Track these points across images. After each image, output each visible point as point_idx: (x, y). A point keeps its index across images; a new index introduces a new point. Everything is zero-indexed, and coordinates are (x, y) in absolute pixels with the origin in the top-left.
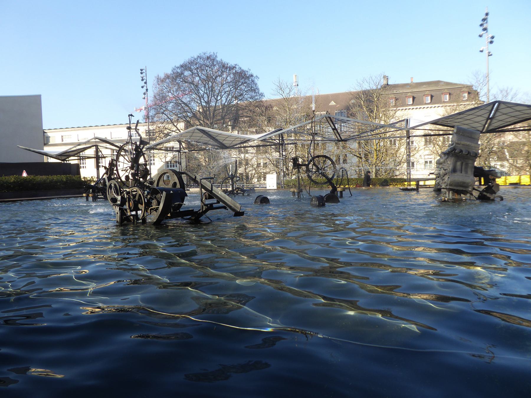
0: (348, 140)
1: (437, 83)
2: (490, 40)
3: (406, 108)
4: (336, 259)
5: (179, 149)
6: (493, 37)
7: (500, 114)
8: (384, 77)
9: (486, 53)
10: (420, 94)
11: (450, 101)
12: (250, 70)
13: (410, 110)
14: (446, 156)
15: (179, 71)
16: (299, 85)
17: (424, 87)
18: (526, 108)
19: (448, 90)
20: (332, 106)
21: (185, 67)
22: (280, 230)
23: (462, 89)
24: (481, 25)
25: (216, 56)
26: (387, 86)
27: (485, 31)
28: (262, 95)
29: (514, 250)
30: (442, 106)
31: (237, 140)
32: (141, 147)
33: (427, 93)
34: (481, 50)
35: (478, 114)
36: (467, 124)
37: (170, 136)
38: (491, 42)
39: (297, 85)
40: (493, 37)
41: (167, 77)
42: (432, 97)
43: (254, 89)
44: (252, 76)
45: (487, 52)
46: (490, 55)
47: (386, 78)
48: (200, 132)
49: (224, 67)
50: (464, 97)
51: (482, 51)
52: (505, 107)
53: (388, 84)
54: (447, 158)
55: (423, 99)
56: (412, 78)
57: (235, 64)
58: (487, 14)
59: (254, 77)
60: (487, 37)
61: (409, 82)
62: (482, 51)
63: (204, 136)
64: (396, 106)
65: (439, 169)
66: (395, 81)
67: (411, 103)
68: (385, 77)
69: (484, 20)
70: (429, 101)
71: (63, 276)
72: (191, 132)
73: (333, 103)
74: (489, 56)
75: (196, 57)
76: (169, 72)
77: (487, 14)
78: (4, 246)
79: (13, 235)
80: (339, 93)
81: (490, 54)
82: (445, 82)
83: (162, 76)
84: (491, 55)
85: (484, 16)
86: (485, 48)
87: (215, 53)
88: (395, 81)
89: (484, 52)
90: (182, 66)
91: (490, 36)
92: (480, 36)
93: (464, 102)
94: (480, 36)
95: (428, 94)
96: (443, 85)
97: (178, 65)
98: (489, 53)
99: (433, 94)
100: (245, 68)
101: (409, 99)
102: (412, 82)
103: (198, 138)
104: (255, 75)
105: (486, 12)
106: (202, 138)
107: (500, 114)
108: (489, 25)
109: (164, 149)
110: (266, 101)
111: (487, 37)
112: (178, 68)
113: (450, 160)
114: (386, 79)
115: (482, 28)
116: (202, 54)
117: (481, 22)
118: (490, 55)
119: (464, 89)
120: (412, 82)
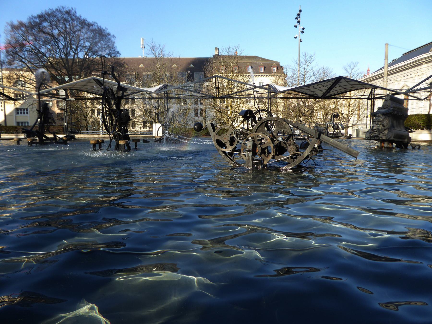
1: (255, 57)
2: (301, 30)
3: (270, 75)
5: (65, 97)
6: (303, 29)
8: (216, 48)
9: (298, 39)
10: (243, 65)
12: (107, 29)
13: (262, 77)
14: (384, 117)
15: (38, 20)
17: (246, 60)
18: (357, 83)
20: (141, 68)
21: (42, 17)
23: (273, 64)
24: (296, 18)
25: (75, 12)
26: (217, 57)
27: (299, 24)
34: (296, 37)
38: (303, 32)
39: (144, 48)
40: (303, 29)
41: (21, 24)
42: (265, 68)
43: (111, 47)
44: (109, 34)
48: (95, 82)
49: (84, 24)
51: (296, 38)
52: (344, 81)
53: (218, 55)
54: (385, 118)
55: (258, 69)
57: (94, 21)
58: (300, 11)
59: (111, 36)
60: (300, 27)
62: (296, 38)
64: (238, 72)
65: (378, 125)
66: (248, 53)
68: (216, 49)
69: (298, 15)
70: (263, 71)
71: (370, 246)
72: (87, 81)
74: (300, 42)
76: (25, 20)
77: (300, 11)
80: (131, 59)
81: (301, 41)
82: (260, 58)
83: (16, 23)
84: (302, 41)
85: (298, 12)
86: (297, 36)
87: (74, 8)
88: (248, 53)
91: (302, 27)
92: (295, 26)
94: (295, 26)
95: (262, 66)
97: (35, 15)
98: (300, 40)
99: (265, 65)
100: (103, 27)
104: (112, 34)
105: (300, 9)
106: (85, 87)
108: (301, 19)
110: (124, 59)
111: (300, 27)
112: (35, 17)
113: (387, 119)
114: (217, 50)
115: (296, 21)
116: (61, 8)
117: (296, 16)
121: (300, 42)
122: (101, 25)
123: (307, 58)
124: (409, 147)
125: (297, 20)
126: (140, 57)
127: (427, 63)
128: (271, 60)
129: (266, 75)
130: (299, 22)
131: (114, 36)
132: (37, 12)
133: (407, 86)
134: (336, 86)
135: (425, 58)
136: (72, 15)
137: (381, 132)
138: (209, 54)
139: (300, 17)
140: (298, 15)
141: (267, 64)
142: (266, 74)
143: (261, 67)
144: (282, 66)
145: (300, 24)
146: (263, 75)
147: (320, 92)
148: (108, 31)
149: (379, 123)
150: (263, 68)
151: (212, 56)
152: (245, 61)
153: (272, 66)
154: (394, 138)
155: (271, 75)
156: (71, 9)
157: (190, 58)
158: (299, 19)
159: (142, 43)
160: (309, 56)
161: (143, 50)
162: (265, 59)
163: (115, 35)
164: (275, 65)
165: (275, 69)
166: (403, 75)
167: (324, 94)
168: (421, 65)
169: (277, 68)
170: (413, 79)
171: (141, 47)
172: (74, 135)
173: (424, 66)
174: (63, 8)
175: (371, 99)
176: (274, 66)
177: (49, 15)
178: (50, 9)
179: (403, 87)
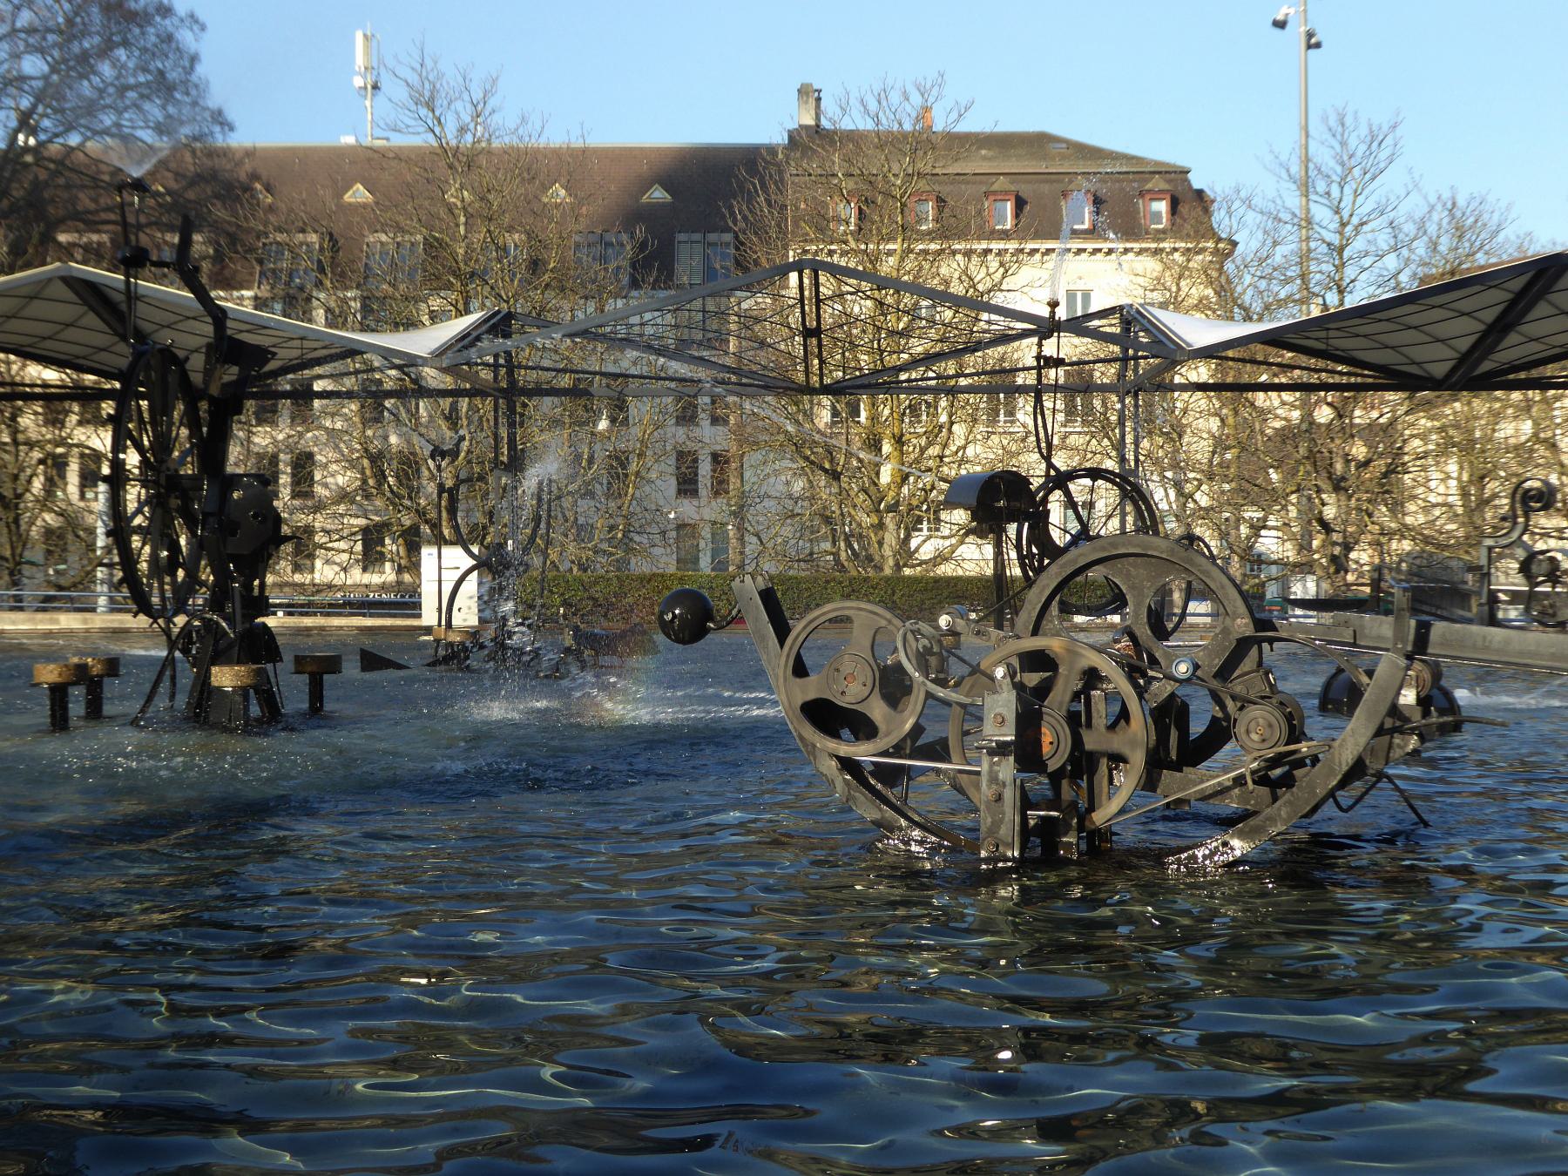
0: (849, 387)
1: (1038, 143)
7: (1549, 310)
9: (1296, 31)
11: (1174, 230)
17: (984, 158)
19: (1012, 183)
23: (1147, 181)
28: (219, 118)
29: (75, 960)
30: (1140, 252)
31: (290, 344)
32: (1112, 370)
33: (1001, 184)
34: (1280, 17)
35: (1464, 305)
36: (1392, 348)
39: (375, 87)
45: (1303, 29)
46: (1312, 44)
47: (809, 94)
50: (1157, 217)
51: (1280, 25)
59: (175, 21)
63: (92, 319)
68: (807, 94)
72: (24, 291)
73: (358, 194)
74: (1309, 47)
78: (543, 1087)
79: (358, 979)
81: (1313, 41)
84: (1318, 45)
86: (1292, 11)
89: (1288, 27)
95: (1006, 192)
96: (1063, 157)
98: (1310, 35)
99: (1026, 190)
101: (999, 204)
103: (45, 329)
106: (70, 334)
107: (1549, 310)
109: (933, 383)
110: (250, 153)
118: (1312, 44)
119: (1157, 183)
121: (1309, 47)
126: (349, 140)
128: (1133, 158)
146: (1090, 246)
153: (1141, 194)
155: (1136, 246)
157: (651, 150)
159: (360, 60)
161: (368, 103)
165: (1162, 207)
169: (1175, 205)
171: (358, 82)
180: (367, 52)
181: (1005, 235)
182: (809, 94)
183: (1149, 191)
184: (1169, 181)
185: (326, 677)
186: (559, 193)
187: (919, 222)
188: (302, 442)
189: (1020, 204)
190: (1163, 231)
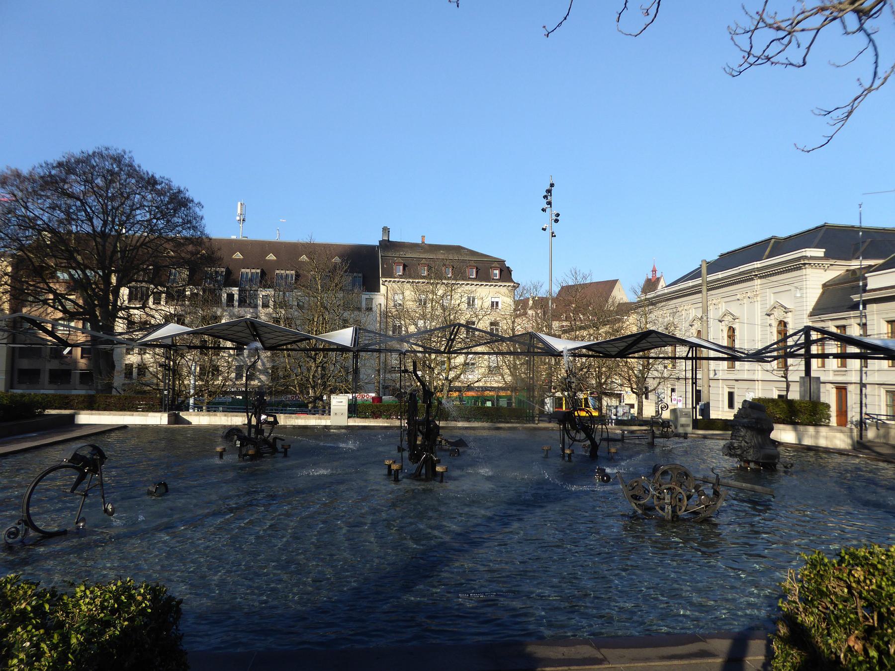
1: (458, 249)
2: (554, 218)
4: (484, 614)
6: (558, 215)
9: (548, 232)
12: (187, 190)
16: (246, 220)
17: (442, 253)
21: (68, 167)
22: (521, 623)
24: (545, 197)
33: (472, 263)
37: (836, 650)
40: (558, 215)
43: (191, 222)
46: (553, 236)
50: (496, 275)
51: (544, 229)
52: (656, 336)
54: (747, 432)
56: (423, 237)
58: (552, 185)
61: (419, 241)
62: (544, 229)
67: (425, 273)
69: (549, 191)
74: (552, 236)
75: (91, 153)
77: (552, 185)
84: (555, 236)
85: (548, 187)
87: (127, 151)
90: (60, 165)
91: (555, 212)
92: (544, 210)
93: (495, 282)
94: (544, 210)
95: (474, 266)
98: (553, 233)
99: (480, 266)
102: (423, 242)
104: (196, 201)
108: (554, 199)
115: (545, 201)
118: (553, 236)
120: (423, 242)
121: (552, 236)
122: (180, 186)
123: (578, 278)
124: (779, 467)
125: (547, 199)
126: (234, 237)
127: (761, 278)
128: (488, 256)
129: (480, 283)
130: (549, 203)
131: (199, 203)
132: (55, 155)
133: (732, 314)
134: (642, 342)
135: (758, 269)
136: (861, 559)
137: (745, 451)
138: (373, 239)
139: (551, 195)
140: (549, 191)
141: (483, 263)
142: (481, 281)
143: (472, 267)
144: (508, 267)
145: (551, 206)
146: (475, 283)
147: (616, 349)
148: (190, 194)
149: (741, 439)
150: (474, 271)
151: (376, 243)
152: (441, 255)
153: (491, 268)
154: (763, 459)
155: (489, 284)
156: (123, 153)
157: (337, 245)
158: (549, 197)
159: (239, 211)
160: (581, 275)
161: (241, 225)
162: (477, 253)
163: (202, 203)
164: (498, 266)
165: (497, 272)
166: (724, 294)
167: (621, 351)
168: (752, 279)
169: (501, 271)
170: (739, 302)
171: (238, 218)
172: (179, 413)
173: (758, 282)
174: (107, 149)
175: (692, 359)
176: (496, 268)
177: (78, 162)
178: (83, 153)
179: (725, 315)
180: (241, 209)
181: (424, 277)
182: (386, 230)
183: (493, 267)
184: (499, 264)
185: (804, 376)
186: (304, 258)
187: (471, 275)
188: (444, 358)
189: (405, 266)
190: (497, 279)
